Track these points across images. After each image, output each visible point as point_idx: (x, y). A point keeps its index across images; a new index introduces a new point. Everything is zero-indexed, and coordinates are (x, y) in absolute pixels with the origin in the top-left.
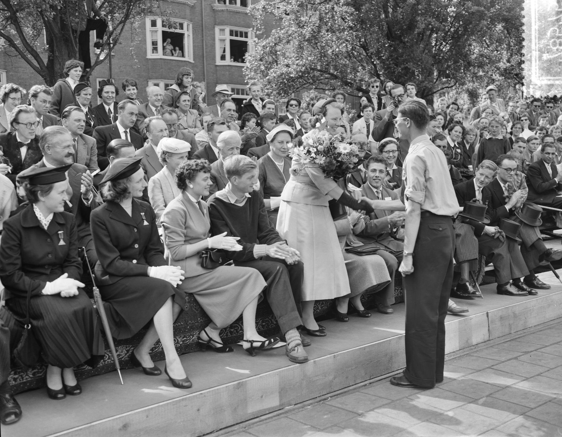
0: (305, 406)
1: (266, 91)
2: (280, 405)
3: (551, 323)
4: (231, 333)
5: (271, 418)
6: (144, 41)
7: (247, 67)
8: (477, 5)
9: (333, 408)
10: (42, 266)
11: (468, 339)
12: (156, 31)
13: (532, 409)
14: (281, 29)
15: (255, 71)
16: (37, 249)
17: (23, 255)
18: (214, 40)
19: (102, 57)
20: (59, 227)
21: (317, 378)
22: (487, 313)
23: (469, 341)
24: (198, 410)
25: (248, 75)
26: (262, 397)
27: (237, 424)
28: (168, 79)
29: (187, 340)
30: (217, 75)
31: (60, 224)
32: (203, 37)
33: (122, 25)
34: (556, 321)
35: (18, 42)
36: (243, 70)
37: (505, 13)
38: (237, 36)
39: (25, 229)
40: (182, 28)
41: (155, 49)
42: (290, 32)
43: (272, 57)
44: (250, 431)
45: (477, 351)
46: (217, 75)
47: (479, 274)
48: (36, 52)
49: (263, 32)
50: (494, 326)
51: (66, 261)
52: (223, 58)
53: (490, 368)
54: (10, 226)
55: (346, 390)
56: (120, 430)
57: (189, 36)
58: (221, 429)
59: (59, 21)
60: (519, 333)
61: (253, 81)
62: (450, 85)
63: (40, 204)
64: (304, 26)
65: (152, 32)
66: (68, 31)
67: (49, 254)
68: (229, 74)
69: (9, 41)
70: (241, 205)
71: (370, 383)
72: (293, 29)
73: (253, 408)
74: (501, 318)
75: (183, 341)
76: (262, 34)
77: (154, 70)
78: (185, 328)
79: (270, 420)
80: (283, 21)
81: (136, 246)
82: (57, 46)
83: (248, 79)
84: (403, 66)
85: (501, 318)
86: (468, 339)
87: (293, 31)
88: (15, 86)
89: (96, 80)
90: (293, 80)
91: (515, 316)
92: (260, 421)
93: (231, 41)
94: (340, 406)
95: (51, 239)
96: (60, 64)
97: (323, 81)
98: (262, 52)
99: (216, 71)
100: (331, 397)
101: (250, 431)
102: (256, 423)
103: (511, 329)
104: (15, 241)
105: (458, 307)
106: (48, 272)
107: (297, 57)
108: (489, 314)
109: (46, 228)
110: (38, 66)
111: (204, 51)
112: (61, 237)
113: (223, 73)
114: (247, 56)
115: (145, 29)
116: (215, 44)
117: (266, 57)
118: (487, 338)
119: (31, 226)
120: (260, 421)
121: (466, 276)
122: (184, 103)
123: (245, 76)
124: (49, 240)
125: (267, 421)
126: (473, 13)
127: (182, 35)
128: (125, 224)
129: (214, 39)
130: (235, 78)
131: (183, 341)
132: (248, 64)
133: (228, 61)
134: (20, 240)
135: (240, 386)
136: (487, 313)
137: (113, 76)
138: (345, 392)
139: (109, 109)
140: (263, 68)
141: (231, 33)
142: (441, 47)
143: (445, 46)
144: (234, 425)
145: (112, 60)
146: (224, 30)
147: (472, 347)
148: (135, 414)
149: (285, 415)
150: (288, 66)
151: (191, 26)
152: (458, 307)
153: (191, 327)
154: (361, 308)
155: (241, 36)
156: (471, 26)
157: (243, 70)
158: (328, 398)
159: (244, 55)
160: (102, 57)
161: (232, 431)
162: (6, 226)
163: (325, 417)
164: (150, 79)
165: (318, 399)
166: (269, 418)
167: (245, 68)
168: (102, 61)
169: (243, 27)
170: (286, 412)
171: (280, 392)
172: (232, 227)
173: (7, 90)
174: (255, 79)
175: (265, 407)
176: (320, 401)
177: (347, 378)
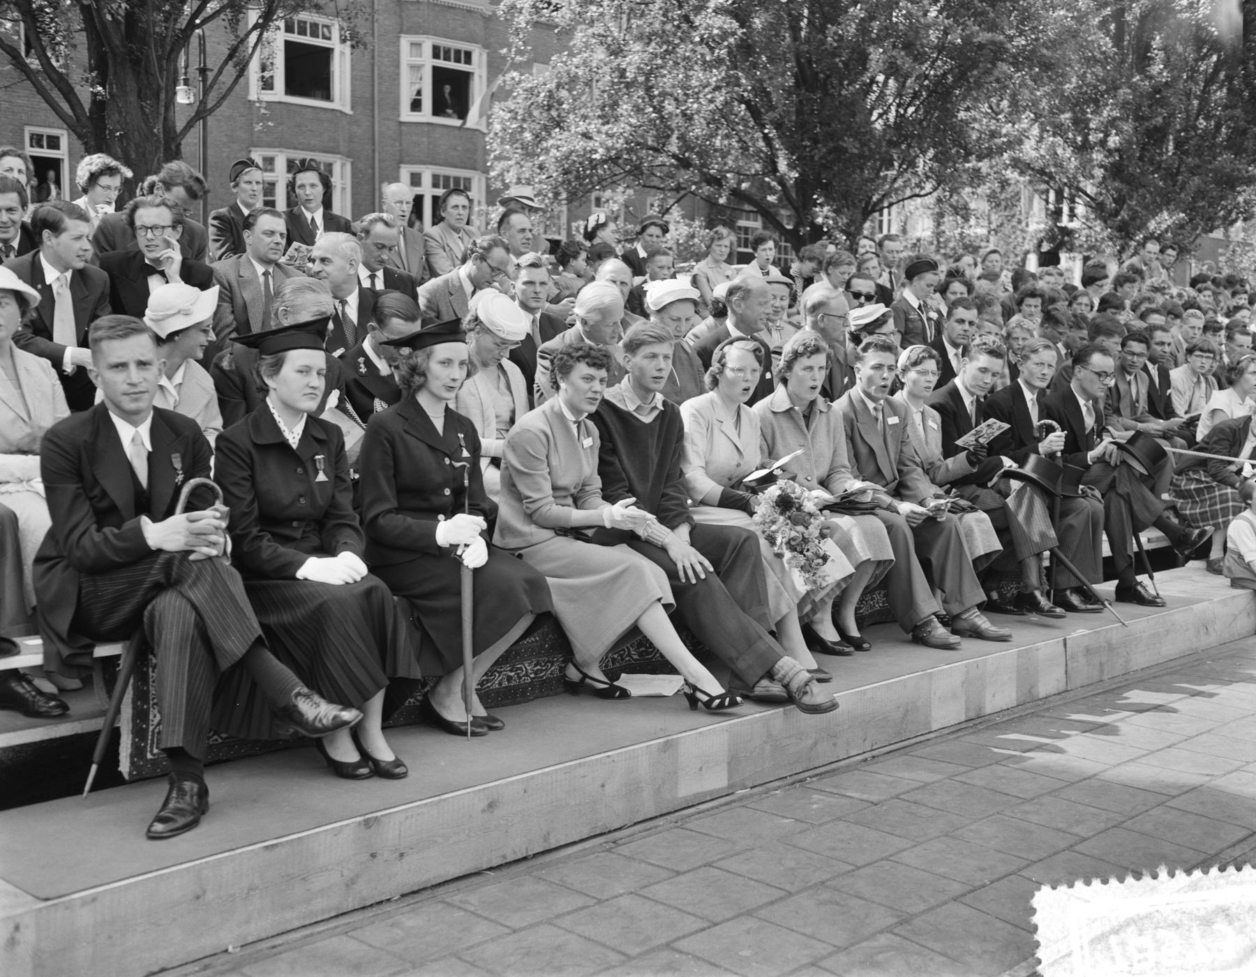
2: (730, 786)
3: (1171, 664)
5: (716, 807)
8: (989, 30)
10: (287, 522)
13: (1174, 797)
14: (571, 55)
17: (258, 496)
18: (397, 66)
26: (701, 769)
27: (662, 815)
28: (295, 148)
29: (541, 671)
30: (401, 145)
31: (318, 441)
32: (373, 58)
34: (1176, 663)
37: (1045, 51)
38: (447, 58)
40: (468, 59)
41: (267, 84)
46: (401, 145)
48: (69, 85)
49: (529, 59)
51: (327, 515)
52: (416, 105)
55: (834, 766)
56: (483, 811)
58: (635, 824)
60: (1116, 680)
62: (923, 192)
67: (301, 496)
68: (429, 143)
73: (687, 788)
75: (536, 673)
81: (447, 492)
82: (115, 73)
85: (1088, 651)
88: (114, 163)
90: (594, 165)
91: (1111, 648)
96: (120, 113)
99: (401, 134)
102: (692, 815)
103: (1102, 671)
105: (993, 628)
106: (298, 535)
109: (295, 447)
110: (70, 112)
111: (375, 88)
112: (320, 466)
113: (415, 139)
116: (398, 74)
118: (1062, 687)
119: (271, 441)
122: (455, 212)
124: (300, 470)
126: (981, 46)
127: (467, 76)
128: (429, 446)
129: (397, 65)
131: (536, 673)
135: (668, 746)
138: (833, 770)
139: (313, 219)
140: (528, 136)
146: (419, 45)
150: (586, 136)
152: (993, 628)
155: (458, 60)
156: (975, 72)
164: (255, 146)
165: (790, 780)
166: (712, 808)
169: (462, 39)
170: (740, 799)
171: (729, 763)
172: (624, 457)
173: (94, 168)
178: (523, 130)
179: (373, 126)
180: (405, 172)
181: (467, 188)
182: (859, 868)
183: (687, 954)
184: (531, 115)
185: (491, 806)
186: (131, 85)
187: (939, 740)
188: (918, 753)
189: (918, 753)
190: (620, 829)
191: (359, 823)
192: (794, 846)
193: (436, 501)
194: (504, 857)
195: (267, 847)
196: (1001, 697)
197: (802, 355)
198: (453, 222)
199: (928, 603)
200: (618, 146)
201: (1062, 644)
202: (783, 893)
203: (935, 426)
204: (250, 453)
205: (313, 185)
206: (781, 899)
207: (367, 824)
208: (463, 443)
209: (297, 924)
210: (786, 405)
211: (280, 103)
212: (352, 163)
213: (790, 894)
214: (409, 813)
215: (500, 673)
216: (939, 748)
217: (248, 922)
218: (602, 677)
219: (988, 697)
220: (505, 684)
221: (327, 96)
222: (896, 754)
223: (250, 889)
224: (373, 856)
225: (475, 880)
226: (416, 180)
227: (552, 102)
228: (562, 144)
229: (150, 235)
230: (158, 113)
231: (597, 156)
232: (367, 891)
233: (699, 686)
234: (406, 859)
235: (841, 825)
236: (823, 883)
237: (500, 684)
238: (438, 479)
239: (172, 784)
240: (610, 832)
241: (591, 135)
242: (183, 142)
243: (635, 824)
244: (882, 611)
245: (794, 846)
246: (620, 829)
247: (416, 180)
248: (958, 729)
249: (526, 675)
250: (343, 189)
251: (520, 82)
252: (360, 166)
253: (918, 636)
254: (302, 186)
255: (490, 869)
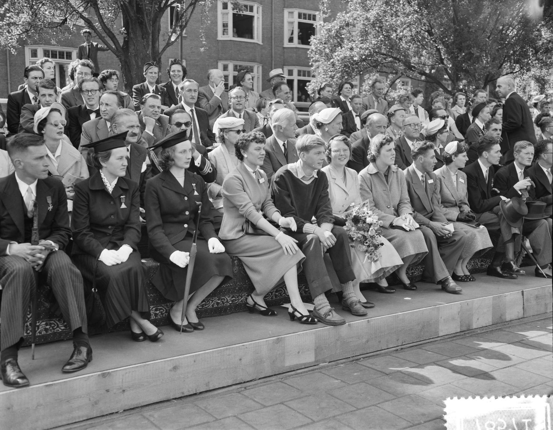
0: (338, 364)
1: (330, 73)
2: (316, 361)
4: (276, 296)
5: (307, 372)
6: (215, 23)
7: (312, 50)
9: (364, 367)
10: (106, 226)
11: (502, 315)
12: (227, 14)
14: (347, 13)
15: (320, 54)
16: (102, 211)
18: (283, 22)
19: (173, 39)
20: (121, 192)
21: (351, 340)
22: (523, 292)
23: (503, 317)
24: (240, 360)
25: (313, 58)
26: (299, 352)
27: (275, 375)
28: (237, 60)
31: (122, 189)
32: (272, 19)
33: (192, 7)
35: (97, 24)
36: (308, 52)
38: (305, 18)
39: (92, 191)
40: (251, 9)
41: (225, 31)
42: (355, 16)
43: (337, 40)
44: (286, 381)
45: (510, 327)
47: (519, 255)
48: (113, 34)
50: (529, 304)
52: (291, 40)
53: (519, 342)
54: (80, 190)
55: (378, 353)
56: (171, 370)
57: (258, 18)
58: (260, 379)
59: (135, 5)
61: (317, 63)
63: (104, 169)
64: (369, 9)
65: (223, 14)
66: (143, 14)
69: (89, 23)
70: (307, 183)
71: (402, 349)
72: (358, 12)
73: (290, 362)
74: (537, 297)
75: (232, 301)
76: (330, 17)
77: (221, 52)
78: (235, 289)
79: (306, 373)
80: (349, 4)
81: (187, 213)
83: (313, 61)
84: (466, 51)
85: (537, 297)
86: (502, 315)
87: (358, 14)
89: (168, 60)
92: (296, 374)
93: (300, 24)
94: (371, 366)
95: (115, 203)
96: (134, 45)
97: (385, 64)
98: (328, 35)
99: (284, 53)
100: (363, 358)
101: (286, 381)
104: (84, 202)
107: (362, 40)
108: (525, 293)
109: (111, 192)
111: (273, 33)
112: (123, 201)
114: (312, 39)
115: (217, 12)
116: (283, 26)
117: (331, 41)
118: (521, 315)
119: (98, 189)
120: (296, 374)
121: (511, 255)
123: (309, 59)
124: (112, 203)
125: (303, 374)
130: (302, 60)
131: (232, 301)
132: (313, 47)
133: (296, 43)
134: (88, 202)
135: (279, 341)
136: (523, 292)
137: (183, 57)
138: (377, 355)
139: (177, 88)
140: (327, 51)
141: (300, 16)
142: (508, 32)
143: (512, 30)
144: (272, 376)
145: (184, 41)
146: (292, 13)
147: (506, 323)
148: (184, 358)
149: (319, 370)
151: (261, 8)
153: (240, 289)
154: (407, 281)
155: (310, 19)
157: (308, 52)
158: (360, 359)
159: (310, 38)
160: (173, 39)
161: (270, 381)
162: (77, 189)
163: (356, 374)
165: (351, 359)
166: (304, 372)
167: (310, 50)
168: (173, 42)
170: (321, 368)
171: (315, 350)
174: (319, 61)
175: (301, 362)
176: (353, 361)
177: (380, 342)
178: (325, 48)
179: (272, 50)
180: (220, 65)
181: (252, 71)
182: (358, 409)
183: (425, 422)
184: (329, 41)
185: (175, 368)
186: (139, 33)
187: (442, 341)
188: (426, 348)
189: (426, 348)
190: (251, 381)
191: (99, 375)
192: (332, 396)
193: (181, 218)
194: (183, 393)
195: (47, 386)
196: (482, 319)
197: (385, 144)
198: (346, 94)
199: (442, 272)
200: (366, 54)
201: (521, 294)
202: (310, 421)
203: (463, 181)
204: (88, 193)
205: (179, 71)
206: (308, 424)
207: (104, 375)
208: (195, 188)
209: (65, 423)
210: (375, 171)
211: (296, 48)
212: (262, 66)
213: (314, 422)
214: (128, 371)
215: (212, 301)
216: (439, 346)
217: (37, 421)
218: (263, 304)
219: (474, 320)
220: (216, 306)
221: (252, 37)
222: (415, 347)
223: (38, 405)
224: (108, 391)
225: (165, 404)
226: (225, 68)
227: (338, 34)
228: (341, 53)
229: (90, 94)
230: (149, 45)
231: (355, 59)
232: (104, 408)
233: (298, 310)
234: (126, 393)
235: (363, 384)
236: (334, 417)
237: (213, 306)
238: (181, 207)
239: (75, 347)
240: (244, 382)
241: (354, 49)
242: (162, 57)
243: (260, 379)
244: (418, 276)
245: (332, 396)
246: (251, 381)
247: (225, 68)
248: (454, 336)
249: (227, 302)
250: (258, 78)
251: (323, 26)
252: (266, 67)
253: (443, 287)
254: (174, 71)
255: (175, 399)
